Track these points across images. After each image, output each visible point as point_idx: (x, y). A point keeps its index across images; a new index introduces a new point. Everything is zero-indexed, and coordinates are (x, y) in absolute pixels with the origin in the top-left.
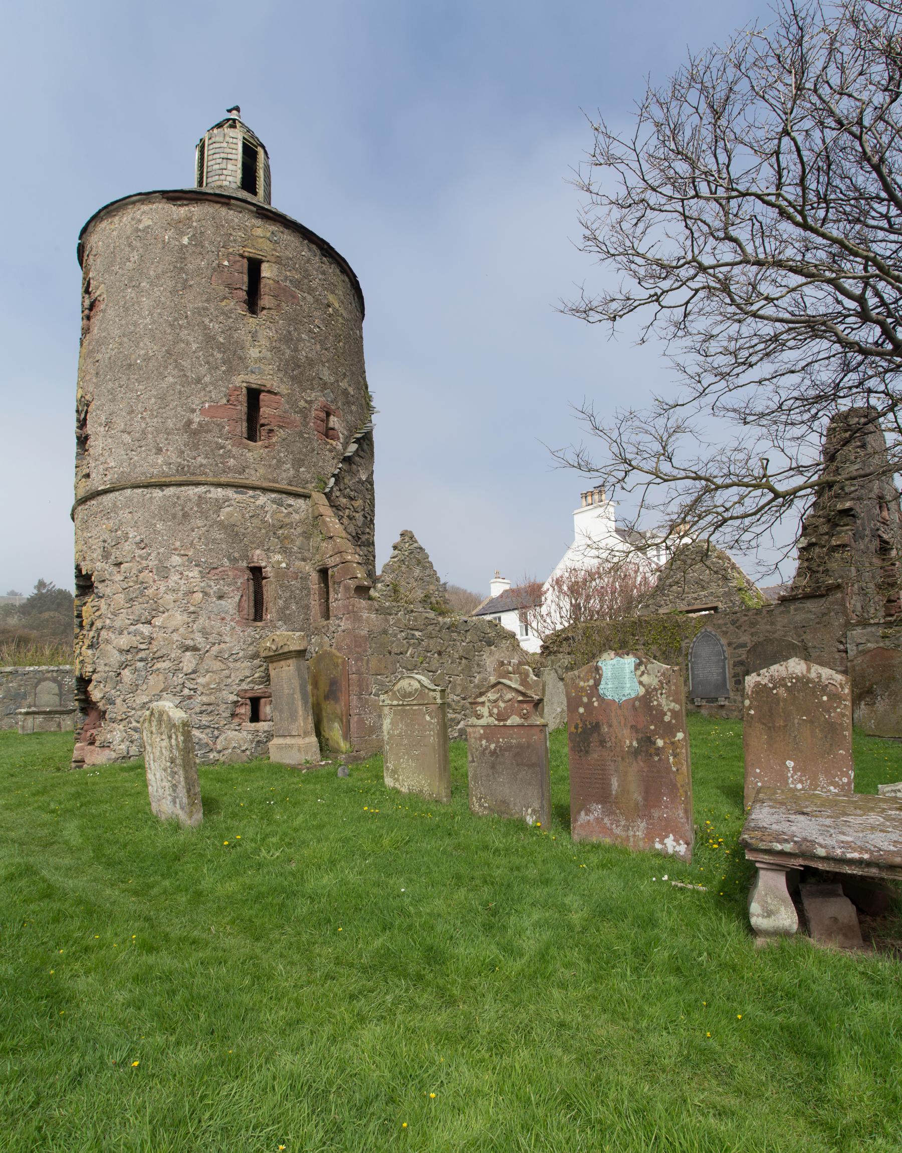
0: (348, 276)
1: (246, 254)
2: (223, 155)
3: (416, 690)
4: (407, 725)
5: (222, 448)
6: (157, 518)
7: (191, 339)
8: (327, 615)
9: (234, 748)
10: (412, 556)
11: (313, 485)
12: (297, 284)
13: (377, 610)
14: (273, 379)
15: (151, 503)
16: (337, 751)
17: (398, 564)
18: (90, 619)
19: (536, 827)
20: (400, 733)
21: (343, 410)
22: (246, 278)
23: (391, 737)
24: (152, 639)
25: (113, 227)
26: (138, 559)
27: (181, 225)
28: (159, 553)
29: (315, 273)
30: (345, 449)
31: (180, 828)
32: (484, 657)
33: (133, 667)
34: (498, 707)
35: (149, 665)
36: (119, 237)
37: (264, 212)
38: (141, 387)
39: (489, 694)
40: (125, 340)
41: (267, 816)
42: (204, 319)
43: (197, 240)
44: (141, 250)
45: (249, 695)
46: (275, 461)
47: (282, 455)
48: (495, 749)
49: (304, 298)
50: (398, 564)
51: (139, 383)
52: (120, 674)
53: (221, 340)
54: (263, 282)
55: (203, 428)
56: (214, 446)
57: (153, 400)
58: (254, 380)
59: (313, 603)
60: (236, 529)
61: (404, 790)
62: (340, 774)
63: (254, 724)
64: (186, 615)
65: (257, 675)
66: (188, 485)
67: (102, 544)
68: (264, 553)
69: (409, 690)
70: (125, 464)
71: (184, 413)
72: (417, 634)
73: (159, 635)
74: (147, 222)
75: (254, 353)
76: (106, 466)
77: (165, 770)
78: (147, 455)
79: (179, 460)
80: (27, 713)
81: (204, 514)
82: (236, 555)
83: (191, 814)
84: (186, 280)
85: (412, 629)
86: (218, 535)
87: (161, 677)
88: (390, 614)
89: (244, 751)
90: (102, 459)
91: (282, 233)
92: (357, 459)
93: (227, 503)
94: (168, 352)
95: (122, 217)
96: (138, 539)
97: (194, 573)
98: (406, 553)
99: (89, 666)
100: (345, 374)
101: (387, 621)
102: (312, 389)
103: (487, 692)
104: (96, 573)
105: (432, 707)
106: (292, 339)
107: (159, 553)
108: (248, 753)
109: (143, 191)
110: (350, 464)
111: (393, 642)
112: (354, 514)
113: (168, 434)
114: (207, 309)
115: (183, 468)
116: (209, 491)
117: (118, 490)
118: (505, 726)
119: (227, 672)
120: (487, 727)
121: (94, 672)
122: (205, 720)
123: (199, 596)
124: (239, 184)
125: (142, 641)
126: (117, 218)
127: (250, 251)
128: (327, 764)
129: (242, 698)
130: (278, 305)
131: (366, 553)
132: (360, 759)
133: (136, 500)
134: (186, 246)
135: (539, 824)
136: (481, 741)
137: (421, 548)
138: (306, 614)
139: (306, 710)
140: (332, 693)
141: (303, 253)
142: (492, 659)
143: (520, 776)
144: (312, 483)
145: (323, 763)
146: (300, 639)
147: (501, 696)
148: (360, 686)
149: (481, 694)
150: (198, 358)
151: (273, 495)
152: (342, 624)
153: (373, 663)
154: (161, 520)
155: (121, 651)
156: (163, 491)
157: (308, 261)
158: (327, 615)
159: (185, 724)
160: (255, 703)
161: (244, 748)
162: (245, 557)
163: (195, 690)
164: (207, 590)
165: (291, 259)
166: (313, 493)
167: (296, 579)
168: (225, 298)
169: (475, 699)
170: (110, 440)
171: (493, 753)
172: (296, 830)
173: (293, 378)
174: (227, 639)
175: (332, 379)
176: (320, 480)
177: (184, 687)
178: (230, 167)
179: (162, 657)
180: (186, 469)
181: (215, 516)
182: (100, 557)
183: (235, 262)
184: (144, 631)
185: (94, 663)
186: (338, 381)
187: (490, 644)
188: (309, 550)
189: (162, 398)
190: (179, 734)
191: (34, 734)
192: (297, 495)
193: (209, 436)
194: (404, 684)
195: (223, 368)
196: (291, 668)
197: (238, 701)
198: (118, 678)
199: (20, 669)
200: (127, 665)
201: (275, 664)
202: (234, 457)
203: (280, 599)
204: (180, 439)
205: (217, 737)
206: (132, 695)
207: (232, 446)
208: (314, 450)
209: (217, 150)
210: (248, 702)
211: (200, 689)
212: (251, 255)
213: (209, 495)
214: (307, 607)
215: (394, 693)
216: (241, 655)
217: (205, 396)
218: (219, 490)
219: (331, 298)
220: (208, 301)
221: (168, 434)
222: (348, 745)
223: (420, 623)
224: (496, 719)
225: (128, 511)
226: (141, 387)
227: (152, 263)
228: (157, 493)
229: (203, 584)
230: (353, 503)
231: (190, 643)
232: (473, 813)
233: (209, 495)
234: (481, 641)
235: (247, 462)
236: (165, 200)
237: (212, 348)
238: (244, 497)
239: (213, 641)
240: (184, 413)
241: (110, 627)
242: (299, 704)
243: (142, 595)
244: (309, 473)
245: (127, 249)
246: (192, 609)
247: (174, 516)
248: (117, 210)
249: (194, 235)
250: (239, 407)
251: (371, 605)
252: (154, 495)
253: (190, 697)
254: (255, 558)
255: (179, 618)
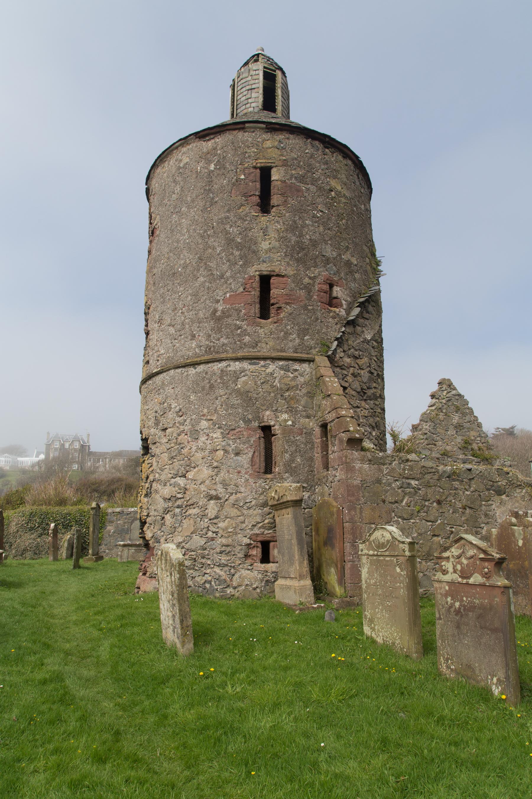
0: (351, 159)
1: (259, 165)
2: (248, 88)
3: (388, 541)
4: (381, 576)
5: (239, 328)
6: (191, 391)
7: (216, 244)
8: (326, 467)
9: (247, 585)
10: (450, 404)
11: (317, 350)
12: (302, 179)
13: (370, 461)
14: (280, 264)
15: (187, 379)
16: (331, 595)
17: (436, 412)
18: (146, 474)
19: (501, 700)
20: (376, 583)
21: (346, 280)
22: (258, 185)
23: (368, 585)
24: (186, 489)
25: (164, 170)
26: (177, 425)
27: (209, 156)
28: (192, 419)
29: (318, 165)
30: (348, 314)
31: (177, 656)
32: (493, 507)
33: (172, 513)
34: (461, 564)
35: (184, 511)
36: (168, 177)
37: (273, 126)
38: (181, 289)
39: (453, 550)
40: (171, 254)
41: (247, 652)
42: (226, 226)
43: (221, 165)
44: (182, 183)
45: (259, 539)
46: (282, 333)
47: (289, 327)
48: (459, 608)
49: (308, 189)
50: (436, 412)
51: (180, 286)
52: (164, 518)
53: (239, 240)
54: (273, 184)
55: (226, 314)
56: (233, 327)
57: (190, 297)
58: (265, 268)
59: (316, 455)
60: (250, 394)
61: (379, 640)
62: (327, 618)
63: (263, 565)
64: (211, 470)
65: (266, 521)
66: (213, 362)
67: (154, 414)
68: (272, 413)
69: (382, 540)
70: (171, 350)
71: (210, 304)
72: (413, 483)
73: (191, 486)
74: (186, 160)
75: (265, 245)
76: (159, 353)
77: (169, 602)
78: (185, 341)
79: (207, 343)
80: (124, 546)
81: (225, 385)
82: (250, 417)
83: (183, 643)
84: (213, 198)
85: (408, 478)
86: (236, 401)
87: (192, 521)
88: (384, 464)
89: (255, 589)
90: (156, 348)
91: (288, 139)
92: (361, 321)
93: (243, 374)
94: (200, 259)
95: (170, 161)
96: (178, 408)
97: (217, 434)
98: (444, 401)
99: (145, 511)
100: (347, 247)
101: (381, 471)
102: (316, 266)
103: (451, 546)
104: (151, 437)
105: (402, 559)
106: (297, 227)
107: (192, 419)
108: (258, 590)
109: (182, 137)
110: (354, 327)
111: (387, 491)
112: (359, 371)
113: (200, 323)
114: (228, 218)
115: (210, 349)
116: (229, 365)
117: (165, 371)
118: (467, 584)
119: (242, 518)
120: (451, 583)
121: (148, 516)
122: (224, 559)
123: (220, 453)
124: (260, 107)
125: (179, 491)
126: (167, 162)
127: (262, 162)
128: (318, 607)
129: (254, 541)
130: (285, 201)
131: (372, 406)
132: (354, 604)
133: (177, 378)
134: (213, 171)
135: (504, 697)
136: (446, 598)
137: (459, 395)
138: (310, 466)
139: (301, 554)
140: (329, 541)
141: (307, 151)
142: (503, 509)
143: (484, 640)
144: (315, 348)
145: (315, 606)
146: (296, 490)
147: (463, 552)
148: (354, 534)
149: (446, 549)
150: (221, 258)
151: (281, 363)
152: (337, 474)
153: (367, 513)
154: (193, 393)
155: (165, 499)
156: (195, 368)
157: (312, 156)
158: (326, 467)
159: (181, 564)
160: (265, 546)
161: (255, 586)
162: (257, 418)
163: (216, 533)
164: (227, 448)
165: (296, 159)
166: (316, 357)
167: (301, 434)
168: (242, 205)
169: (440, 553)
170: (161, 333)
171: (458, 612)
172: (265, 669)
173: (298, 260)
174: (242, 490)
175: (335, 254)
176: (324, 345)
177: (208, 530)
178: (254, 95)
179: (193, 505)
180: (212, 349)
181: (234, 385)
182: (153, 425)
183: (249, 174)
184: (181, 483)
185: (148, 508)
186: (340, 255)
187: (499, 492)
188: (313, 408)
189: (195, 295)
190: (176, 572)
191: (128, 562)
192: (302, 361)
193: (229, 321)
194: (378, 534)
195: (241, 263)
196: (290, 516)
197: (251, 544)
198: (163, 522)
199: (125, 510)
200: (169, 511)
201: (279, 512)
202: (249, 335)
203: (287, 453)
204: (208, 326)
205: (233, 575)
206: (171, 535)
207: (247, 326)
208: (318, 319)
209: (244, 85)
210: (259, 545)
211: (221, 532)
212: (262, 165)
213: (229, 369)
214: (311, 459)
215: (370, 544)
216: (253, 503)
217: (227, 288)
218: (237, 363)
219: (333, 183)
220: (228, 211)
221: (200, 323)
222: (343, 591)
223: (417, 471)
224: (460, 576)
225: (171, 386)
226: (181, 289)
227: (189, 192)
228: (192, 371)
229: (223, 444)
230: (358, 361)
231: (213, 493)
232: (440, 674)
233: (229, 369)
234: (488, 490)
235: (259, 337)
236: (198, 139)
237: (232, 248)
238: (257, 367)
239: (231, 491)
240: (210, 304)
241: (159, 480)
242: (296, 548)
243: (180, 453)
244: (313, 340)
245: (173, 184)
246: (215, 464)
247: (203, 388)
248: (166, 157)
249: (218, 161)
250: (253, 293)
251: (364, 456)
252: (190, 373)
253: (213, 539)
254: (266, 418)
255: (206, 472)
